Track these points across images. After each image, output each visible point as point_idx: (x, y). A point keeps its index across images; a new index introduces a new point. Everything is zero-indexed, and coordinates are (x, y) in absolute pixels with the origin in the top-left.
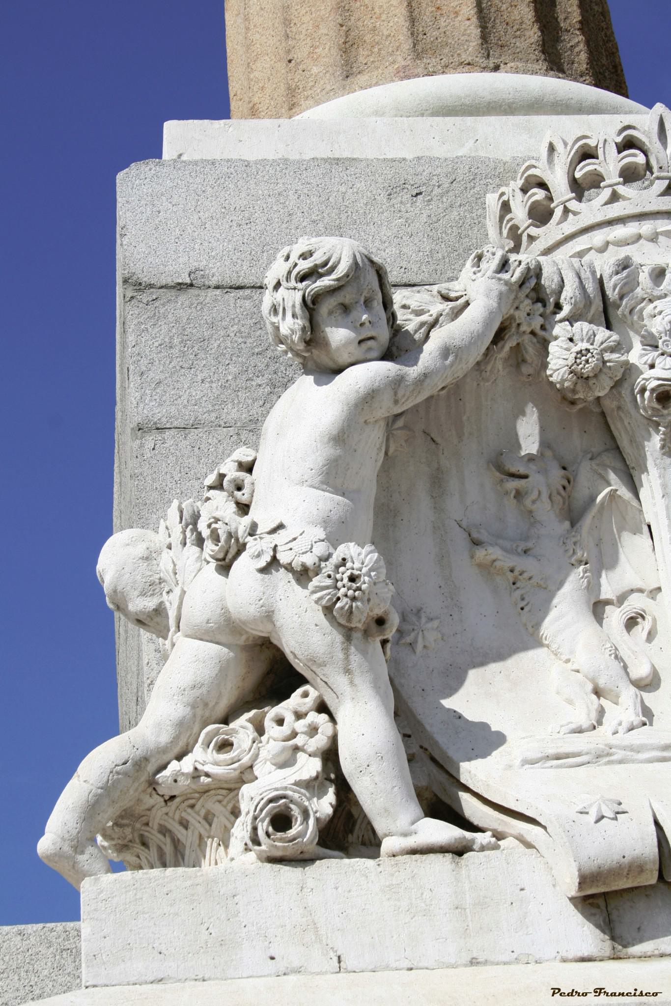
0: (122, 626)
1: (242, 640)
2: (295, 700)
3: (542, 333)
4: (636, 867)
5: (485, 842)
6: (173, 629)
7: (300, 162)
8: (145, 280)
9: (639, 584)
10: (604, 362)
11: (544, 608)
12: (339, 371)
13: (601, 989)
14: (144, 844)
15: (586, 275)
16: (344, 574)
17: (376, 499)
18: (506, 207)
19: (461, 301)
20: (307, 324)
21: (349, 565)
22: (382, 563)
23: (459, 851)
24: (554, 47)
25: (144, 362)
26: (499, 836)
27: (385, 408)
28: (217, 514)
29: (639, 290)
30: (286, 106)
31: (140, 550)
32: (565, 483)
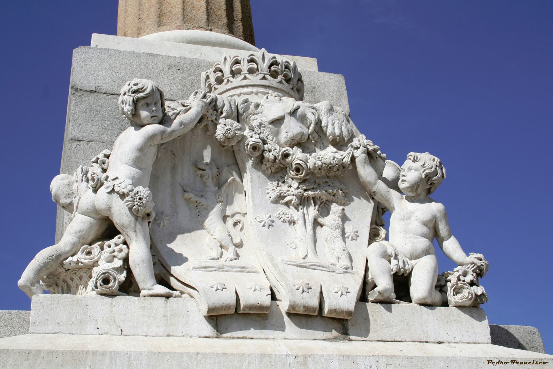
0: (59, 209)
1: (99, 217)
2: (116, 239)
3: (215, 121)
4: (228, 307)
5: (177, 294)
6: (75, 210)
7: (139, 53)
8: (79, 88)
9: (239, 211)
10: (235, 134)
11: (206, 216)
12: (143, 126)
13: (514, 360)
14: (57, 285)
15: (232, 103)
17: (152, 172)
18: (208, 77)
19: (189, 107)
21: (139, 194)
22: (151, 194)
23: (167, 297)
24: (231, 26)
25: (76, 116)
26: (182, 293)
27: (158, 141)
28: (95, 172)
29: (250, 110)
30: (136, 34)
31: (66, 182)
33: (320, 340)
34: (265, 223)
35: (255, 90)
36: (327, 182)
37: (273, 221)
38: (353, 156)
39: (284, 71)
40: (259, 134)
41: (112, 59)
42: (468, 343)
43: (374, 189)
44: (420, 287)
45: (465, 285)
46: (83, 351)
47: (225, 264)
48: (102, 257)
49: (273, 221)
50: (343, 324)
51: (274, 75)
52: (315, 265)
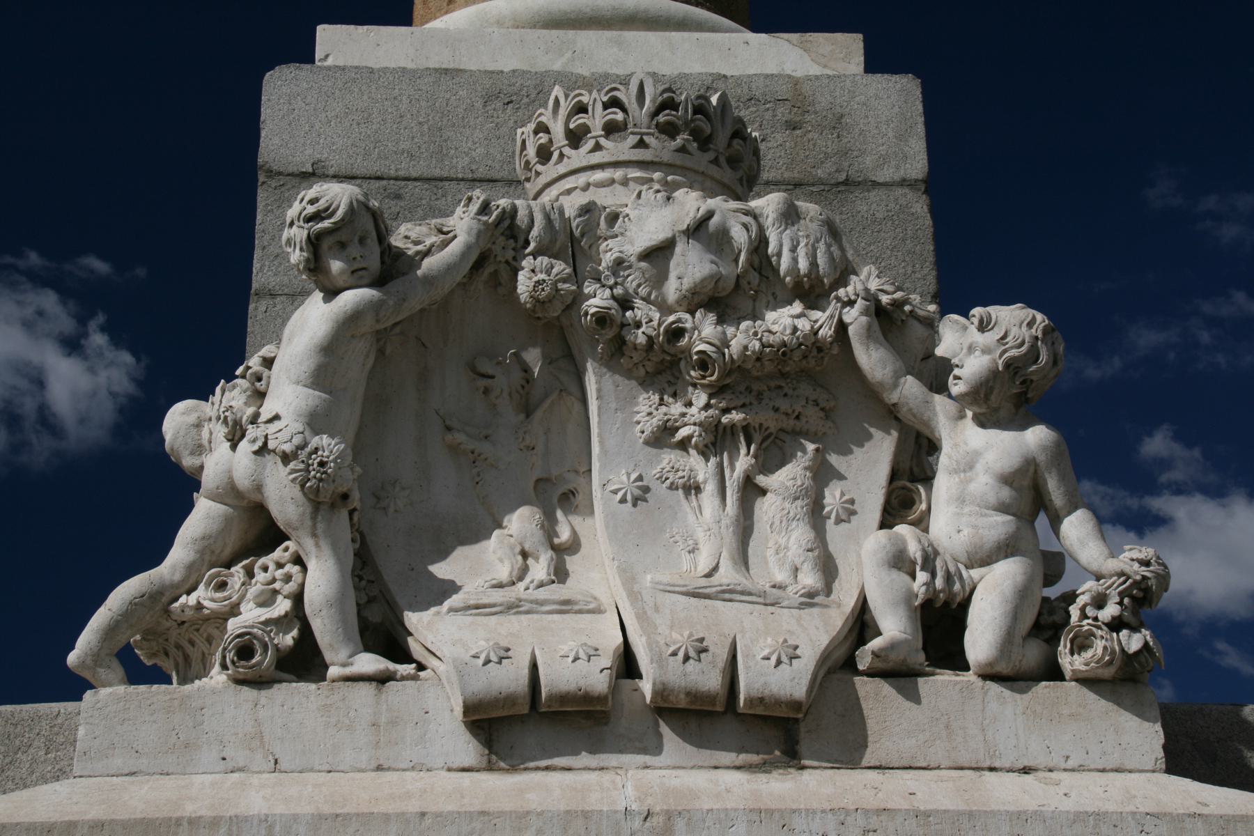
1: (245, 503)
2: (278, 554)
4: (510, 700)
7: (414, 71)
10: (557, 290)
14: (167, 654)
15: (555, 216)
16: (315, 460)
19: (451, 235)
20: (311, 257)
23: (382, 679)
27: (368, 324)
31: (192, 418)
32: (524, 383)
33: (728, 768)
36: (780, 387)
37: (646, 489)
38: (840, 321)
39: (692, 120)
40: (611, 288)
41: (351, 92)
42: (1103, 771)
43: (893, 397)
44: (982, 636)
45: (1099, 628)
46: (170, 819)
47: (523, 595)
48: (249, 596)
49: (646, 489)
50: (780, 732)
51: (669, 130)
52: (731, 592)
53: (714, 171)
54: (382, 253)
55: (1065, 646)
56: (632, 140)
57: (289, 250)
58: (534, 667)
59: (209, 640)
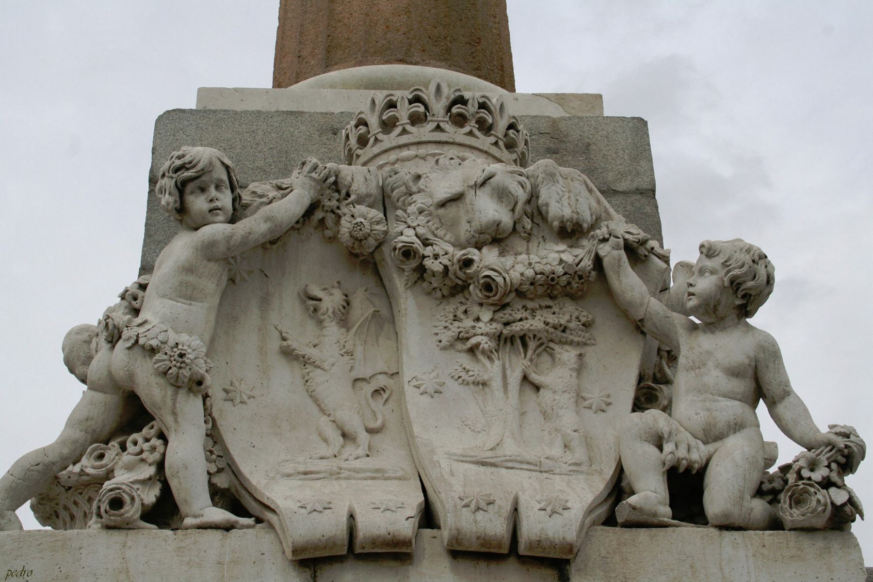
4: (331, 543)
21: (180, 347)
23: (228, 528)
32: (345, 304)
34: (421, 385)
35: (422, 151)
36: (550, 307)
45: (812, 486)
51: (460, 120)
53: (494, 151)
54: (234, 200)
55: (785, 502)
56: (432, 125)
57: (160, 196)
58: (352, 517)
59: (90, 500)
